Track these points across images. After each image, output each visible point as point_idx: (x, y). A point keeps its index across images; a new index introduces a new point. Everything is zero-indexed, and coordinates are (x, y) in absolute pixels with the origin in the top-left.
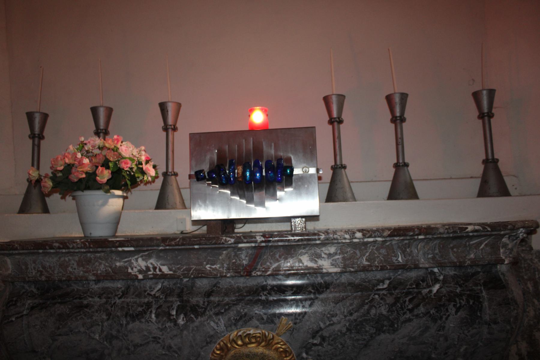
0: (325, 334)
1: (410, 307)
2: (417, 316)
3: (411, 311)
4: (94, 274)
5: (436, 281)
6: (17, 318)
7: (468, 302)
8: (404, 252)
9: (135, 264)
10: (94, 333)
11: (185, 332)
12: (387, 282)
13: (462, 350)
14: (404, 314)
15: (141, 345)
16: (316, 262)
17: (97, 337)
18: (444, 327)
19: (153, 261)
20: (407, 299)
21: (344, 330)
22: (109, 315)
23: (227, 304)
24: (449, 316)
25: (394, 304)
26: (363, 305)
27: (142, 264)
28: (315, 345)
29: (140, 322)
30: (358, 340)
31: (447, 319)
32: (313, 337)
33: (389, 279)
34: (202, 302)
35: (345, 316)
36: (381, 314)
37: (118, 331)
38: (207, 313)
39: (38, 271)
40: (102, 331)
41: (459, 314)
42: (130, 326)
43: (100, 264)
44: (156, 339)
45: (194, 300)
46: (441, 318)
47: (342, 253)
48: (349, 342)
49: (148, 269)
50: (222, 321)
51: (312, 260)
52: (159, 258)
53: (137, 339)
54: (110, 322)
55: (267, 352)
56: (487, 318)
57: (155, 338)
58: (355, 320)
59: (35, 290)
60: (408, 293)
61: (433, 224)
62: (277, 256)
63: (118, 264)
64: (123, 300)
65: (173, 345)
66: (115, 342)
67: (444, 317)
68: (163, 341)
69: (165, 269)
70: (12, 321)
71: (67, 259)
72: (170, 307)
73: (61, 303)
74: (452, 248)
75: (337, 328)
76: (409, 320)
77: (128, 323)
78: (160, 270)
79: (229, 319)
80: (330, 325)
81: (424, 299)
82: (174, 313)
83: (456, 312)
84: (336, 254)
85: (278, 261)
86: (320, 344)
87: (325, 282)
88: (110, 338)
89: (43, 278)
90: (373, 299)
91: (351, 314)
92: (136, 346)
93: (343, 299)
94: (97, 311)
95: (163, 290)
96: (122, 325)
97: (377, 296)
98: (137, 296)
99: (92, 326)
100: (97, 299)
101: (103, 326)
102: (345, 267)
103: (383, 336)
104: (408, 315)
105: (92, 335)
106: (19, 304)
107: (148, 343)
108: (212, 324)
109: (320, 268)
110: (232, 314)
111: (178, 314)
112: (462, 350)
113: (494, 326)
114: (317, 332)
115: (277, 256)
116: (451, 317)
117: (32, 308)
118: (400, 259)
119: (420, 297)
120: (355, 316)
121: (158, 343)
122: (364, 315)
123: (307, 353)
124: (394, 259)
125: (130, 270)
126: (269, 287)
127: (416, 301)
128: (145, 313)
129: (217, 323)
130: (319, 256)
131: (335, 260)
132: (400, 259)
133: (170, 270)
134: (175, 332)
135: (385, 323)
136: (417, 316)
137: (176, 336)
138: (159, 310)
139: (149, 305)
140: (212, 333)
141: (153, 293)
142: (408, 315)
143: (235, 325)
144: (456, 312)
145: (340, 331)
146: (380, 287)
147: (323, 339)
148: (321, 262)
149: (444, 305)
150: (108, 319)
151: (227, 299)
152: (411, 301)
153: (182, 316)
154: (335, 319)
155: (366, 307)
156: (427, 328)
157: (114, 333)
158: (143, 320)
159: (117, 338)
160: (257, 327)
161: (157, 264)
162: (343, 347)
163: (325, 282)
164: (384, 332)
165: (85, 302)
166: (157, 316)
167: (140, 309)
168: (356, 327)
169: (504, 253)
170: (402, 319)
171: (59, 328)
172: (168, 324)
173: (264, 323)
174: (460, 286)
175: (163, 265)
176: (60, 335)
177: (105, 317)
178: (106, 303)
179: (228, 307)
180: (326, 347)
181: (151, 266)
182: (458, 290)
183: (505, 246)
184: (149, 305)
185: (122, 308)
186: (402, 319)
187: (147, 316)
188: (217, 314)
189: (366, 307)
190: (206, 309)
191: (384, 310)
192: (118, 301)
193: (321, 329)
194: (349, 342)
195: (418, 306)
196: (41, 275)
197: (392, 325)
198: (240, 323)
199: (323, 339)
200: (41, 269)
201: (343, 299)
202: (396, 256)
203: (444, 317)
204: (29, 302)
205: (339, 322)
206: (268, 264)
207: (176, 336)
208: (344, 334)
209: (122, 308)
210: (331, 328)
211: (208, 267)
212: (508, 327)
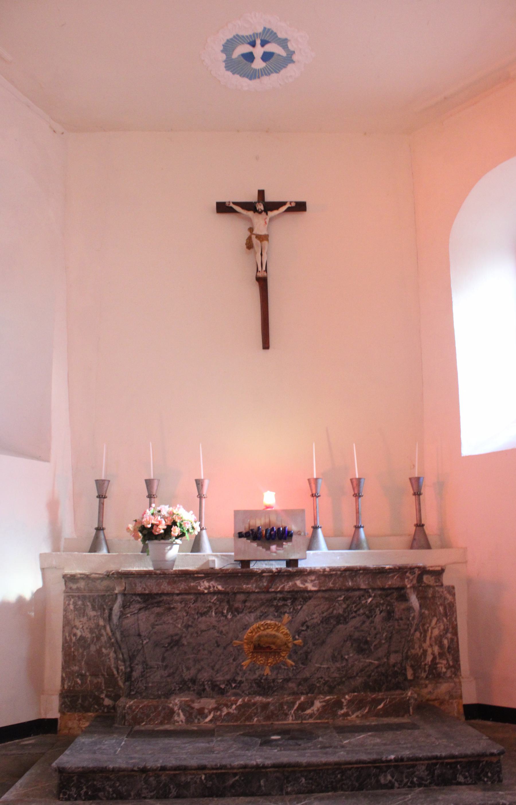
0: (309, 624)
1: (355, 610)
2: (359, 615)
3: (356, 612)
4: (178, 590)
5: (370, 596)
6: (131, 615)
7: (387, 607)
8: (352, 580)
9: (202, 584)
10: (178, 623)
11: (231, 623)
12: (343, 597)
13: (384, 635)
14: (352, 613)
15: (205, 631)
16: (304, 585)
17: (179, 626)
18: (373, 622)
19: (212, 583)
20: (354, 606)
21: (319, 622)
22: (187, 613)
23: (255, 607)
24: (376, 615)
25: (347, 608)
26: (329, 608)
27: (206, 584)
28: (303, 631)
29: (206, 617)
30: (327, 628)
31: (375, 617)
32: (302, 625)
33: (344, 594)
34: (241, 607)
35: (320, 614)
36: (339, 613)
37: (192, 622)
38: (244, 611)
39: (143, 588)
40: (183, 622)
41: (382, 614)
42: (200, 619)
43: (181, 584)
44: (214, 627)
45: (236, 605)
46: (372, 616)
47: (319, 579)
48: (322, 629)
49: (210, 587)
50: (253, 616)
51: (302, 583)
52: (216, 581)
53: (203, 627)
54: (188, 617)
55: (277, 634)
56: (397, 617)
57: (214, 626)
58: (326, 617)
59: (140, 600)
60: (353, 603)
61: (431, 567)
62: (283, 581)
63: (192, 584)
64: (194, 605)
65: (224, 630)
66: (190, 629)
67: (374, 616)
68: (219, 628)
69: (220, 587)
70: (128, 617)
71: (161, 581)
72: (223, 609)
73: (157, 607)
74: (379, 578)
75: (315, 621)
76: (354, 617)
77: (198, 618)
78: (217, 588)
79: (256, 615)
80: (311, 619)
81: (362, 606)
82: (225, 612)
83: (381, 613)
84: (315, 580)
85: (283, 583)
86: (306, 630)
87: (309, 596)
88: (187, 627)
89: (147, 592)
90: (335, 605)
91: (323, 613)
92: (202, 631)
93: (318, 605)
94: (180, 611)
95: (217, 599)
96: (195, 619)
97: (337, 604)
98: (203, 602)
99: (177, 620)
100: (179, 604)
101: (183, 620)
102: (320, 587)
103: (340, 626)
104: (354, 614)
105: (177, 625)
106: (131, 607)
107: (210, 629)
108: (247, 618)
109: (306, 588)
110: (258, 613)
111: (227, 613)
112: (384, 635)
113: (400, 621)
114: (305, 623)
115: (283, 581)
116: (377, 616)
117: (140, 609)
118: (350, 584)
119: (361, 605)
120: (325, 614)
121: (215, 629)
122: (330, 614)
123: (299, 636)
124: (347, 584)
125: (199, 588)
126: (278, 598)
127: (358, 606)
128: (209, 612)
129: (250, 618)
130: (306, 581)
131: (315, 584)
132: (350, 584)
133: (223, 587)
134: (225, 623)
135: (342, 618)
136: (359, 615)
137: (226, 625)
138: (217, 610)
139: (210, 607)
140: (246, 623)
141: (212, 601)
142: (354, 614)
143: (260, 618)
144: (381, 613)
145: (317, 622)
146: (339, 599)
147: (308, 627)
148: (307, 585)
149: (374, 609)
150: (187, 616)
151: (255, 605)
152: (355, 607)
153: (230, 613)
154: (314, 616)
155: (331, 609)
156: (364, 622)
157: (190, 623)
158: (208, 616)
159: (191, 626)
160: (272, 620)
161: (215, 584)
162: (319, 632)
163: (309, 596)
164: (341, 624)
165: (172, 606)
166: (216, 613)
167: (205, 610)
168: (325, 620)
169: (407, 582)
170: (351, 616)
171: (156, 621)
172: (222, 618)
173: (276, 618)
174: (383, 599)
175: (219, 585)
176: (157, 625)
177: (185, 614)
178: (185, 606)
179: (256, 609)
180: (309, 632)
181: (211, 586)
182: (382, 602)
183: (408, 578)
184: (210, 607)
185: (195, 609)
186: (351, 616)
187: (210, 613)
188: (250, 612)
189: (331, 609)
190: (243, 609)
191: (341, 611)
192: (192, 606)
193: (306, 621)
194: (322, 629)
195: (359, 609)
196: (145, 590)
197: (345, 619)
198: (263, 617)
199: (308, 627)
200: (144, 586)
201: (318, 605)
202: (348, 582)
203: (374, 616)
204: (138, 606)
205: (316, 618)
206: (278, 585)
207: (226, 625)
208: (319, 625)
209: (195, 609)
210: (312, 621)
211: (244, 586)
212: (408, 622)
